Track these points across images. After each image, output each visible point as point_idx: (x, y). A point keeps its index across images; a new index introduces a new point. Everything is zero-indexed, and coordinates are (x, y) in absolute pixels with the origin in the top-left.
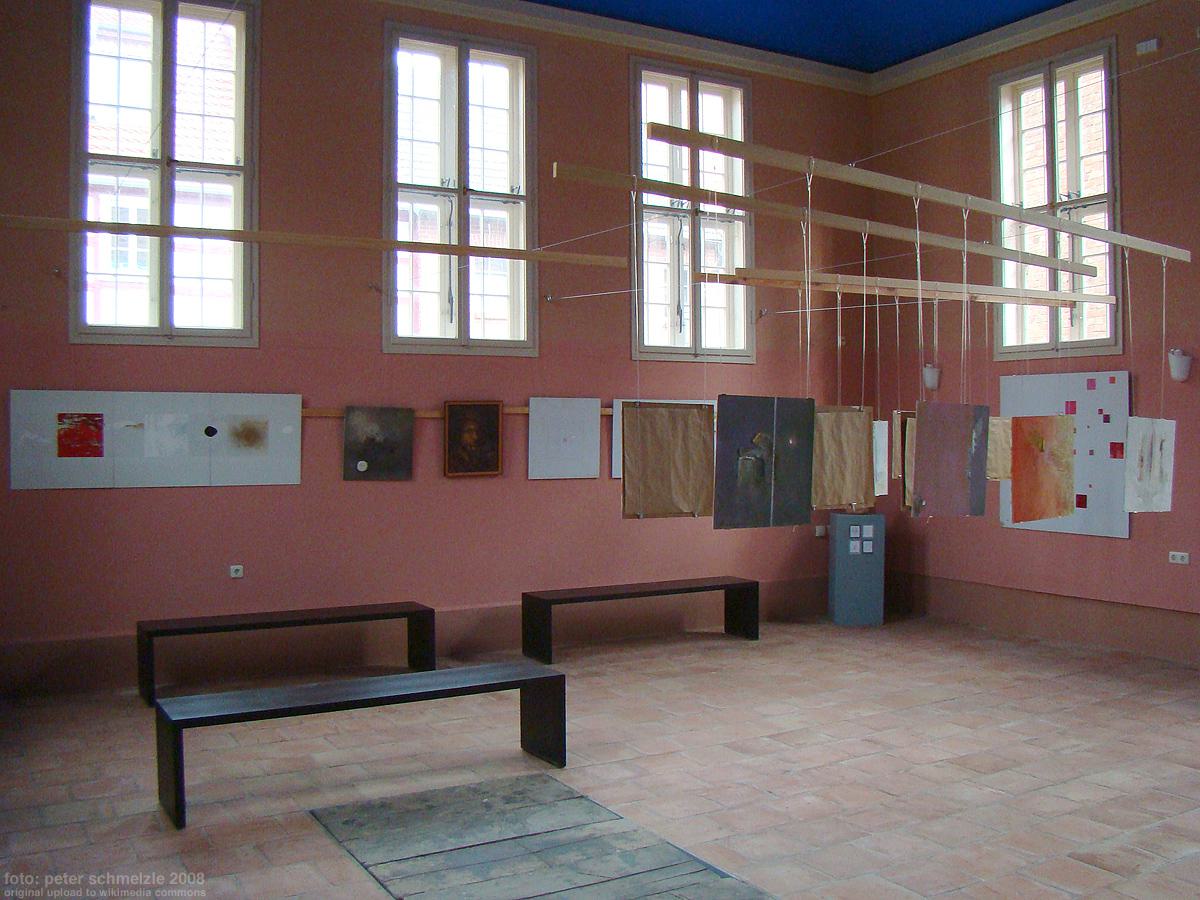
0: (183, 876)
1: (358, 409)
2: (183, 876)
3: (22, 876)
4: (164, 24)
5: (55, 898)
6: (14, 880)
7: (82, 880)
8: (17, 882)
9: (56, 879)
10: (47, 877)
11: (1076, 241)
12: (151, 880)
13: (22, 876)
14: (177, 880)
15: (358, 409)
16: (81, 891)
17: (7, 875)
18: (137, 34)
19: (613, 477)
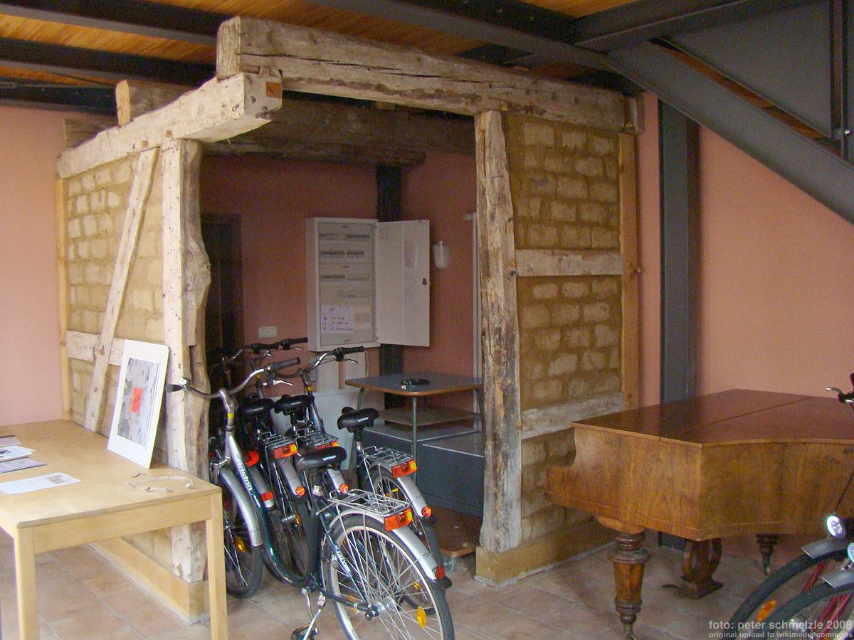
0: (842, 623)
1: (599, 323)
2: (836, 623)
3: (721, 623)
4: (165, 411)
5: (825, 639)
6: (716, 625)
7: (764, 625)
8: (718, 627)
9: (746, 625)
10: (739, 624)
11: (70, 225)
12: (813, 626)
13: (721, 623)
14: (832, 626)
15: (599, 323)
16: (764, 634)
17: (711, 623)
18: (833, 77)
19: (427, 344)
